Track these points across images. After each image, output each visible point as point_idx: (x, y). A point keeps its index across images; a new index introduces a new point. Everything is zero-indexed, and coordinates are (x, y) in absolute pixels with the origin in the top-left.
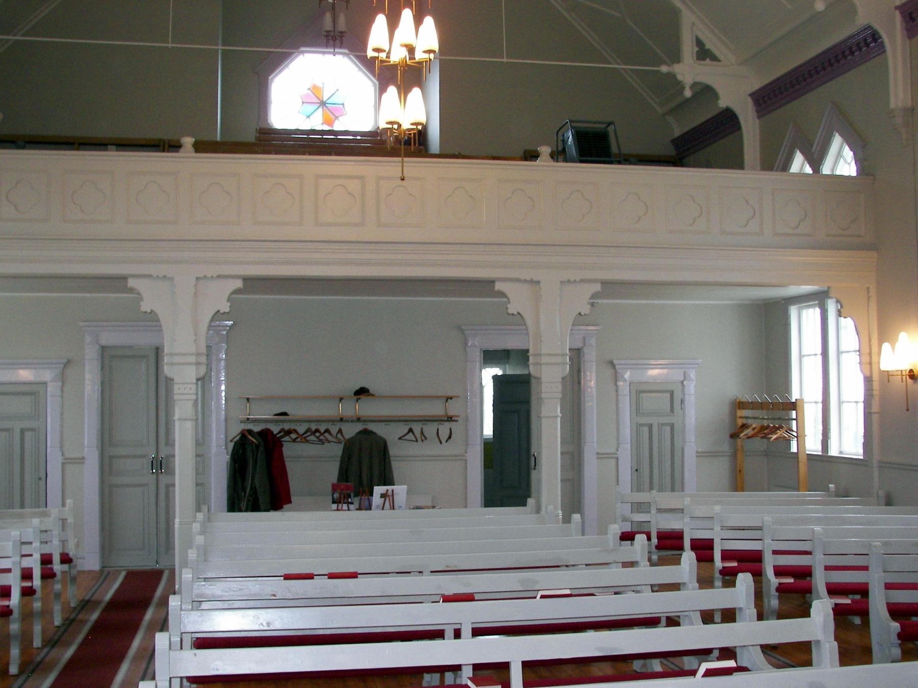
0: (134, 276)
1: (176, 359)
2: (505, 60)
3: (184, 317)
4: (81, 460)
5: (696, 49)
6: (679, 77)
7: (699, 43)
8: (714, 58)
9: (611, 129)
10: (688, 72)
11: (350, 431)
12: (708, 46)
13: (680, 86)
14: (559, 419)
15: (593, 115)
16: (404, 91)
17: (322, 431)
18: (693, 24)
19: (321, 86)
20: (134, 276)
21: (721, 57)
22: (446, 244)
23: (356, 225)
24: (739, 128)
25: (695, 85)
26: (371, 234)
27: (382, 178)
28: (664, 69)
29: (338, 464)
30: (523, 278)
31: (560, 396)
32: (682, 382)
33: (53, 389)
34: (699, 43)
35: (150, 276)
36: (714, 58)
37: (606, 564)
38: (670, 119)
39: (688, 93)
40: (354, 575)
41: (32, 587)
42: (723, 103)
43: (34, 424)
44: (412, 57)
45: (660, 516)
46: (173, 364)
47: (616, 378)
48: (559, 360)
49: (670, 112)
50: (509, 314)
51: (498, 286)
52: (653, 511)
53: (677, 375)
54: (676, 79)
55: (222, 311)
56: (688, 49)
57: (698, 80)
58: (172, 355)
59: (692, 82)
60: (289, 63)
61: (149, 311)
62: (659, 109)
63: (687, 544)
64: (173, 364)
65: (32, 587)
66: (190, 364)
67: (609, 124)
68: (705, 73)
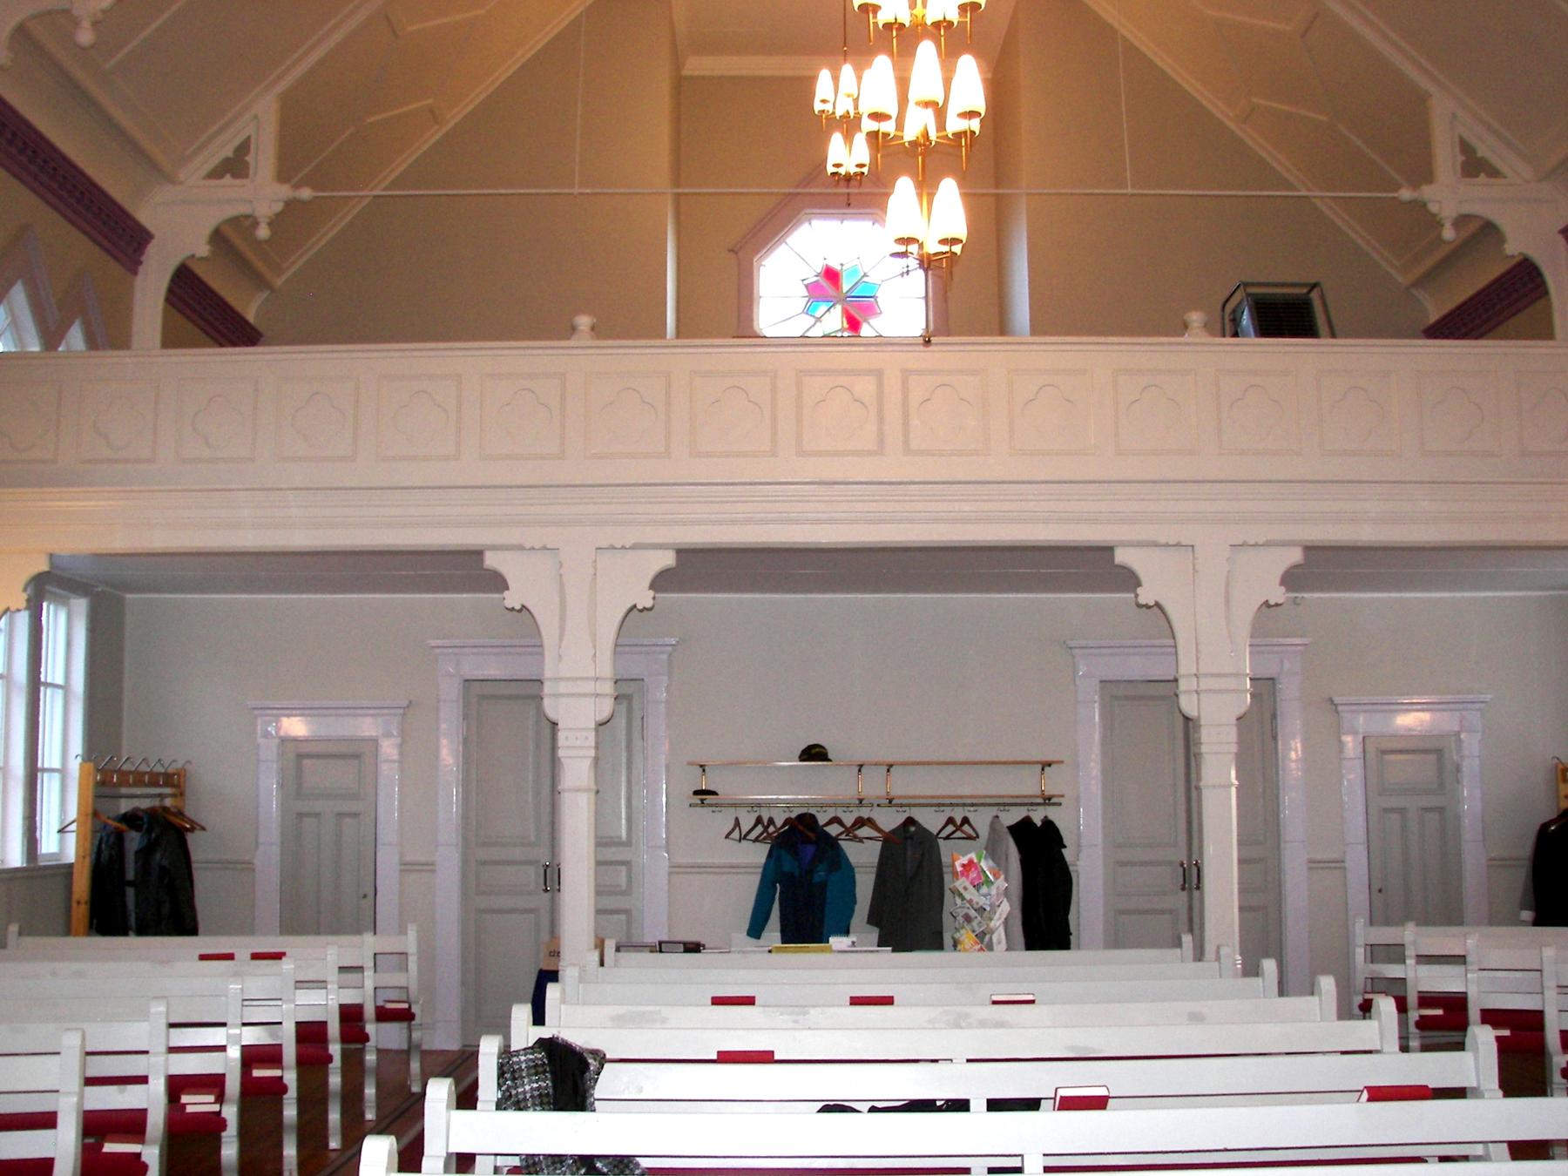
0: (495, 548)
1: (563, 688)
2: (1130, 191)
3: (578, 612)
4: (429, 867)
5: (1461, 158)
6: (1433, 208)
7: (1466, 148)
8: (1494, 173)
9: (1314, 295)
10: (1449, 197)
11: (890, 820)
12: (1482, 151)
13: (1435, 223)
14: (1234, 790)
15: (1281, 273)
16: (926, 187)
17: (849, 823)
18: (1454, 116)
19: (838, 268)
20: (495, 548)
21: (1504, 169)
22: (1030, 482)
23: (869, 453)
24: (1546, 293)
25: (1462, 220)
26: (891, 467)
27: (911, 372)
28: (1405, 194)
29: (873, 877)
30: (1163, 540)
31: (1234, 748)
32: (1458, 734)
33: (389, 749)
34: (1466, 148)
35: (520, 548)
36: (1494, 173)
37: (739, 763)
38: (1419, 294)
39: (1448, 233)
40: (726, 1058)
41: (281, 1078)
42: (1514, 247)
43: (354, 806)
44: (941, 125)
45: (1425, 971)
46: (557, 696)
47: (1338, 731)
48: (1231, 683)
49: (1420, 282)
50: (1139, 606)
51: (1121, 557)
52: (1410, 962)
53: (1448, 722)
54: (1428, 211)
55: (640, 607)
56: (1445, 159)
57: (1467, 209)
58: (558, 679)
59: (1454, 215)
60: (787, 234)
61: (518, 607)
62: (1400, 279)
63: (1474, 1014)
64: (557, 696)
65: (281, 1078)
66: (585, 695)
67: (1314, 286)
68: (1477, 199)
